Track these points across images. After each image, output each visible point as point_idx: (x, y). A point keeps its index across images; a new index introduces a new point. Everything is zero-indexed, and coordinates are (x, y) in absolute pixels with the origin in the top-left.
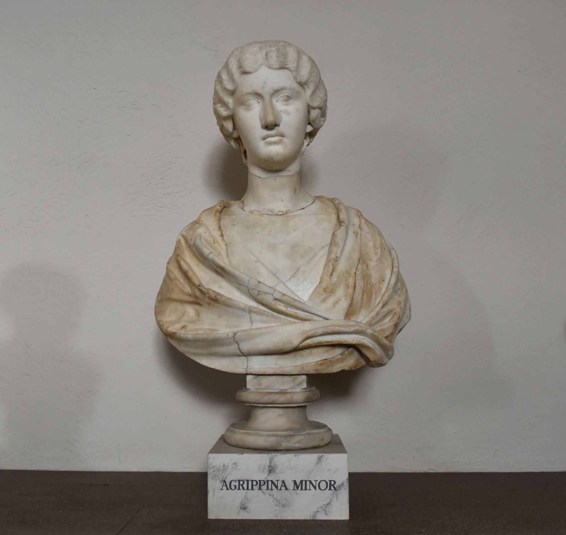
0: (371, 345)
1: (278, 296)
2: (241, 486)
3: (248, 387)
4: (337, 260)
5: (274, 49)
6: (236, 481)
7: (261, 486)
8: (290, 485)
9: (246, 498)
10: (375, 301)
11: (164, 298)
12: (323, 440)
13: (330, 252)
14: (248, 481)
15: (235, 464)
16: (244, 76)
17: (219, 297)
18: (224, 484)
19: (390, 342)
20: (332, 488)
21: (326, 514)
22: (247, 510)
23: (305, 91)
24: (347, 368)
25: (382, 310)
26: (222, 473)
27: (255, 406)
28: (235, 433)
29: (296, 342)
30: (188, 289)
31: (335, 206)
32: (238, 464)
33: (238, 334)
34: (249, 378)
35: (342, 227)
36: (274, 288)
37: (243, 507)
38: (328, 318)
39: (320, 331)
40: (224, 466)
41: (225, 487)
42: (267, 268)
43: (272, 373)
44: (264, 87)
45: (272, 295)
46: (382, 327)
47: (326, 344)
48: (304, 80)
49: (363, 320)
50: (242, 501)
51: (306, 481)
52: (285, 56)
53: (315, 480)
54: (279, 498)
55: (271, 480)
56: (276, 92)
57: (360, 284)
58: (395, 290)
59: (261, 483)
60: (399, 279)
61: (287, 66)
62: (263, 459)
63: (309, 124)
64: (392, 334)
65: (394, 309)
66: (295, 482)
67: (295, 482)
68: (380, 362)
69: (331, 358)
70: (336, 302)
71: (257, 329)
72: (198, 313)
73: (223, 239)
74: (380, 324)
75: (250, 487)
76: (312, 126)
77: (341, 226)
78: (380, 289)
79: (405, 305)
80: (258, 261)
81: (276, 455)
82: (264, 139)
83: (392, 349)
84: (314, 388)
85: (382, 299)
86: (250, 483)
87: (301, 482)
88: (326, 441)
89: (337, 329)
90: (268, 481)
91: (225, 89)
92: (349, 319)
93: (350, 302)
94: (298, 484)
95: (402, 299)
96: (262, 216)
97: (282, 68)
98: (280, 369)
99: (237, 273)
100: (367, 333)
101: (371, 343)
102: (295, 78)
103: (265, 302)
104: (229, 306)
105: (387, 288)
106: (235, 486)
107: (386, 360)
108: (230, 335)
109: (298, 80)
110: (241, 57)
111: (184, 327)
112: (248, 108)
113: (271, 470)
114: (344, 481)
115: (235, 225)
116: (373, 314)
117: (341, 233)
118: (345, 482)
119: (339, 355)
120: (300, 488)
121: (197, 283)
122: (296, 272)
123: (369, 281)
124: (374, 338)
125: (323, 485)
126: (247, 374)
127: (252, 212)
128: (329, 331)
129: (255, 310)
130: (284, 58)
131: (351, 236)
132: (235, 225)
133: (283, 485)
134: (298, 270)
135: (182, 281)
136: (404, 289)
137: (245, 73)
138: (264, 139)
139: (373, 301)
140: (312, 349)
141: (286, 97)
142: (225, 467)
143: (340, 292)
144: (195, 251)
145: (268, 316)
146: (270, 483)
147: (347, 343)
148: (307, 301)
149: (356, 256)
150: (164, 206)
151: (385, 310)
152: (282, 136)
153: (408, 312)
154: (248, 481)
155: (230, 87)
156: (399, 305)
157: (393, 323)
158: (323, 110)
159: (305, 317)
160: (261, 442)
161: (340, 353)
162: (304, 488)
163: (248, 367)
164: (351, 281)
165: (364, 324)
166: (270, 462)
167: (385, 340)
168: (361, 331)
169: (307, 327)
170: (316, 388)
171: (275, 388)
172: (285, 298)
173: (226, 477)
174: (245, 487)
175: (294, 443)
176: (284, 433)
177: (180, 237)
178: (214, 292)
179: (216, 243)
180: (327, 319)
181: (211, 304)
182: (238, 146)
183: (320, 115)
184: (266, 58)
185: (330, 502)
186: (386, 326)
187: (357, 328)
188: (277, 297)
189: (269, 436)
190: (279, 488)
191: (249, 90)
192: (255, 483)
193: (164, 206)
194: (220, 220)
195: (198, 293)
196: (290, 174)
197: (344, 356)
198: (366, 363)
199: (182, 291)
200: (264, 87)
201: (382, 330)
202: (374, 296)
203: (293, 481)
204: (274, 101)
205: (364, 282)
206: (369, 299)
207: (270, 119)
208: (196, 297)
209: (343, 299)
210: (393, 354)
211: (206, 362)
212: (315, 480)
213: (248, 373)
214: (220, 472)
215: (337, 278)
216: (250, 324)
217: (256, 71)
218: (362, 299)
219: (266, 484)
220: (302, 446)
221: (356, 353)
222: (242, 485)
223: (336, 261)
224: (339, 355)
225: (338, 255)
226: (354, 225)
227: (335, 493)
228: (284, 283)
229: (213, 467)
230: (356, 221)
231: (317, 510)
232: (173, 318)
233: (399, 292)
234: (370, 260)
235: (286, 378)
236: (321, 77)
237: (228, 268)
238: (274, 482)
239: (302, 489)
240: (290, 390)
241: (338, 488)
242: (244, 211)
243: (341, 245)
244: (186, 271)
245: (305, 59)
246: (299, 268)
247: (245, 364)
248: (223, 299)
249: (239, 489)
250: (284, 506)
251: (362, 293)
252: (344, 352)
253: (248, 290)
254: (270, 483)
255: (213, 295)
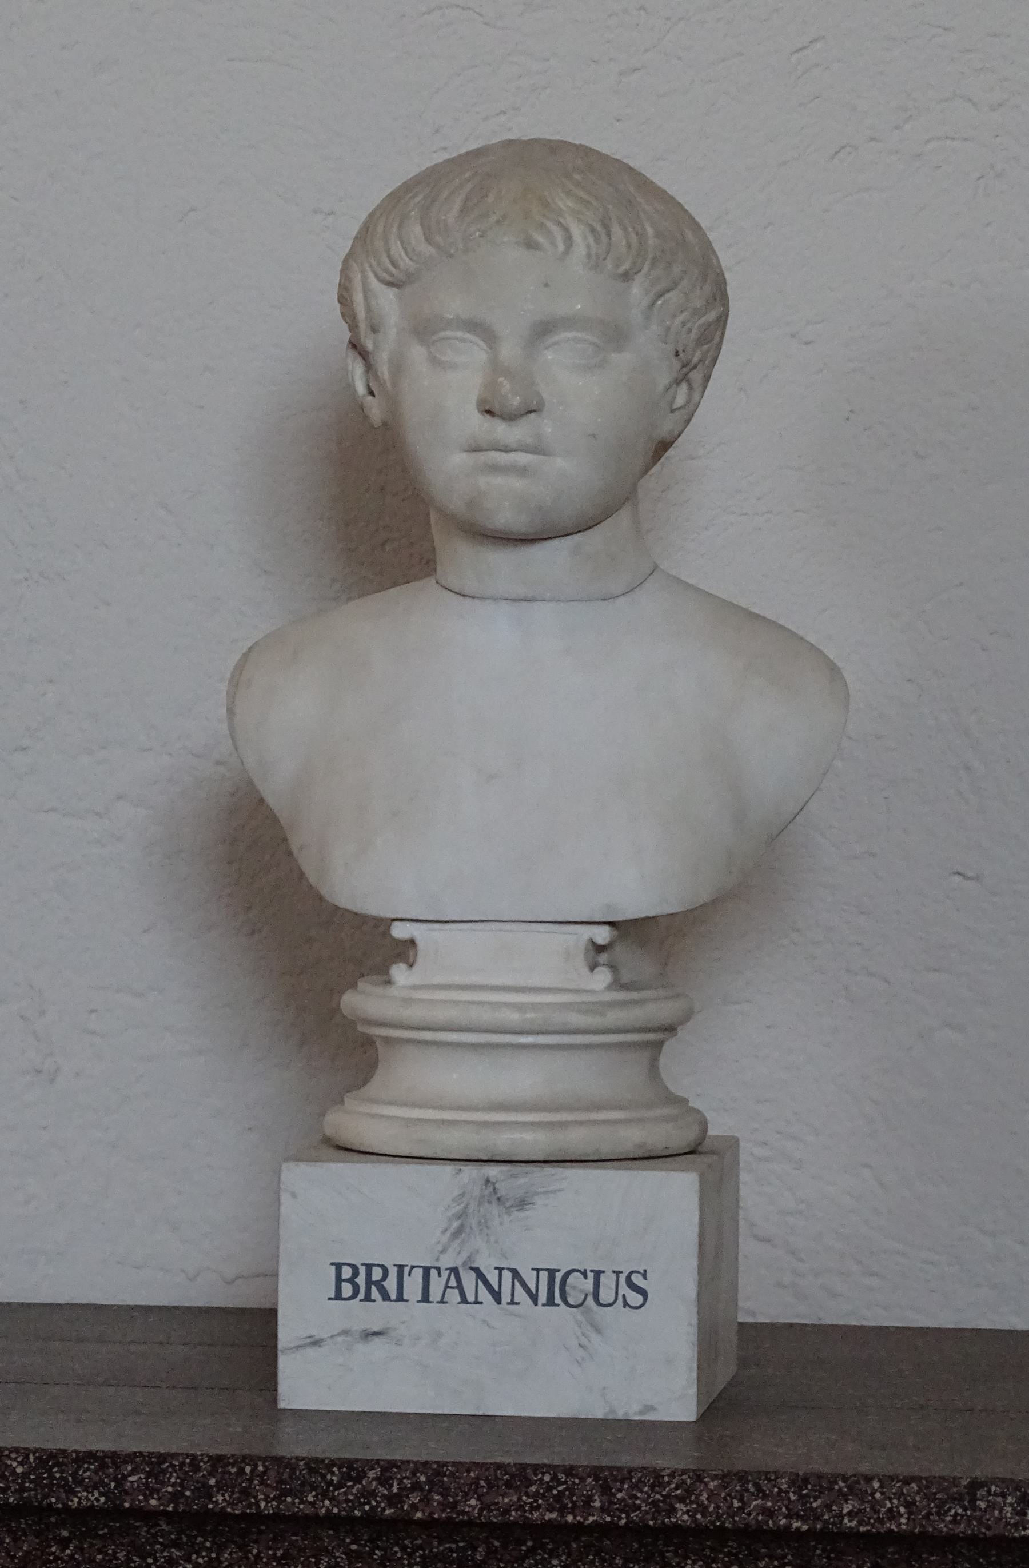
2: (373, 1288)
6: (585, 1274)
18: (453, 1283)
20: (375, 1293)
53: (614, 1272)
203: (334, 1267)
222: (379, 1285)
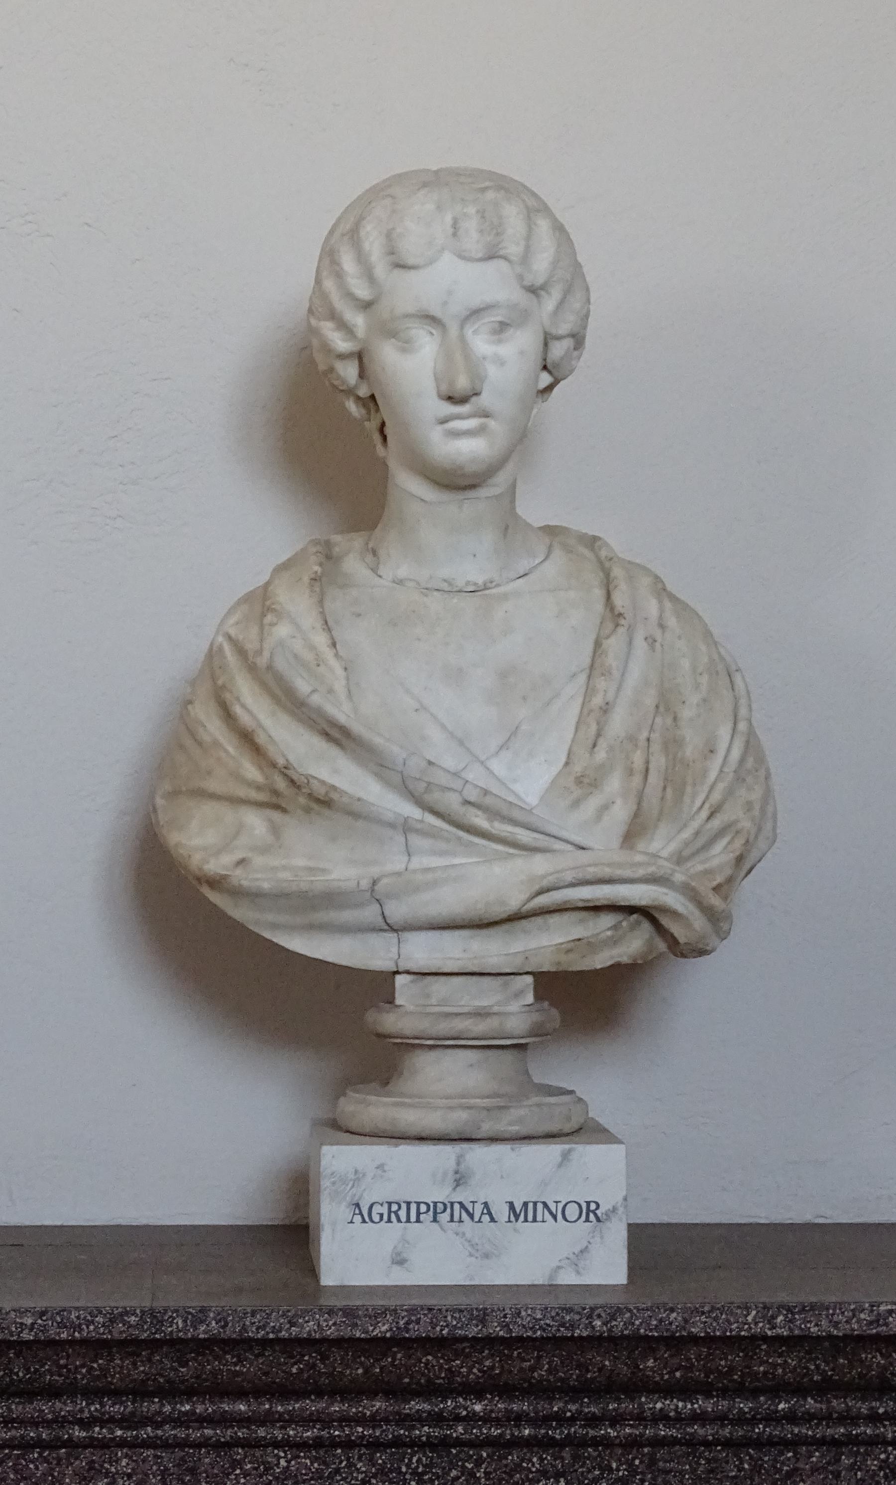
0: (680, 908)
1: (472, 795)
3: (399, 1001)
4: (606, 709)
5: (471, 210)
6: (382, 1205)
7: (438, 1215)
8: (502, 1212)
9: (404, 1240)
10: (693, 802)
11: (184, 789)
12: (569, 1119)
13: (589, 691)
14: (408, 1204)
15: (381, 1167)
16: (397, 271)
17: (335, 796)
18: (357, 1211)
19: (725, 898)
21: (578, 1273)
22: (406, 1265)
23: (539, 302)
24: (625, 960)
25: (709, 826)
26: (353, 1186)
27: (408, 1044)
28: (370, 1104)
29: (515, 901)
30: (251, 771)
31: (601, 563)
32: (386, 1168)
33: (385, 881)
34: (400, 980)
35: (621, 630)
36: (463, 775)
37: (398, 1258)
38: (585, 846)
39: (569, 877)
40: (356, 1172)
41: (359, 1216)
42: (443, 727)
43: (456, 971)
44: (445, 303)
45: (461, 792)
46: (707, 866)
47: (581, 904)
48: (540, 281)
49: (663, 848)
50: (395, 1247)
51: (535, 1204)
52: (498, 230)
53: (555, 1202)
54: (476, 1240)
55: (459, 1200)
56: (475, 313)
57: (659, 761)
58: (739, 778)
59: (438, 1209)
60: (752, 745)
61: (501, 253)
62: (447, 1154)
63: (545, 368)
64: (730, 880)
65: (736, 822)
66: (511, 1206)
67: (511, 1206)
68: (701, 946)
69: (593, 936)
70: (605, 808)
71: (427, 870)
72: (275, 830)
73: (337, 655)
74: (702, 856)
75: (413, 1217)
76: (550, 372)
77: (617, 625)
78: (705, 773)
79: (763, 811)
80: (422, 708)
81: (470, 1148)
82: (443, 421)
83: (729, 917)
84: (546, 1004)
85: (707, 797)
86: (413, 1208)
87: (525, 1204)
88: (573, 1125)
89: (607, 872)
90: (452, 1204)
91: (349, 296)
92: (632, 848)
93: (635, 807)
94: (518, 1211)
95: (756, 795)
96: (426, 596)
97: (490, 257)
98: (476, 962)
99: (378, 740)
100: (673, 882)
101: (683, 904)
102: (520, 278)
103: (441, 808)
104: (355, 815)
105: (721, 771)
106: (381, 1215)
107: (713, 940)
108: (365, 884)
109: (527, 283)
110: (393, 229)
111: (241, 862)
112: (407, 346)
113: (460, 1179)
114: (617, 1203)
115: (359, 615)
116: (687, 834)
117: (615, 644)
118: (619, 1204)
119: (609, 929)
120: (522, 1218)
121: (281, 762)
122: (509, 738)
123: (679, 755)
124: (691, 893)
125: (572, 1212)
126: (397, 972)
127: (400, 582)
128: (588, 877)
129: (419, 826)
130: (498, 234)
131: (640, 644)
132: (359, 615)
133: (485, 1211)
134: (515, 732)
135: (231, 749)
136: (762, 773)
137: (401, 266)
138: (443, 421)
139: (687, 799)
140: (547, 916)
141: (497, 326)
142: (358, 1176)
143: (614, 784)
144: (278, 692)
145: (448, 840)
146: (457, 1207)
147: (627, 904)
148: (537, 805)
149: (650, 701)
150: (120, 516)
151: (716, 823)
152: (486, 415)
153: (769, 826)
154: (408, 1204)
155: (363, 292)
156: (748, 810)
157: (732, 855)
158: (578, 339)
159: (534, 844)
160: (434, 1121)
161: (609, 926)
162: (530, 1218)
163: (399, 956)
164: (638, 759)
165: (666, 859)
166: (458, 1164)
167: (711, 895)
168: (661, 877)
169: (540, 865)
170: (551, 1005)
171: (463, 1003)
172: (488, 800)
173: (361, 1197)
174: (403, 1217)
175: (505, 1124)
176: (486, 1102)
177: (220, 639)
178: (323, 782)
179: (321, 663)
180: (583, 848)
181: (312, 809)
182: (363, 411)
183: (572, 347)
184: (454, 235)
185: (587, 1247)
186: (715, 862)
187: (651, 869)
188: (472, 799)
189: (451, 1108)
190: (476, 1218)
191: (411, 309)
192: (423, 1208)
193: (120, 516)
194: (321, 602)
195: (281, 784)
196: (497, 491)
197: (620, 932)
198: (669, 948)
199: (237, 777)
200: (445, 303)
201: (708, 872)
202: (689, 789)
204: (469, 332)
205: (667, 756)
206: (680, 794)
207: (462, 383)
208: (276, 793)
209: (619, 801)
210: (730, 929)
211: (298, 944)
212: (555, 1202)
213: (400, 970)
214: (347, 1185)
215: (607, 752)
216: (406, 858)
217: (431, 262)
218: (662, 798)
219: (449, 1210)
220: (524, 1130)
221: (646, 925)
222: (396, 1213)
223: (605, 712)
224: (609, 929)
225: (610, 696)
226: (646, 619)
227: (598, 1228)
228: (482, 763)
229: (332, 1174)
230: (652, 607)
231: (560, 1264)
232: (211, 838)
233: (749, 779)
234: (684, 702)
235: (486, 980)
236: (579, 259)
237: (356, 728)
238: (466, 1205)
239: (526, 1220)
240: (496, 1009)
241: (604, 1217)
242: (380, 576)
243: (616, 674)
244: (250, 730)
245: (543, 225)
246: (517, 728)
247: (394, 950)
248: (345, 799)
249: (389, 1221)
250: (487, 1256)
251: (662, 784)
252: (621, 922)
253: (403, 781)
254: (457, 1207)
255: (320, 791)
